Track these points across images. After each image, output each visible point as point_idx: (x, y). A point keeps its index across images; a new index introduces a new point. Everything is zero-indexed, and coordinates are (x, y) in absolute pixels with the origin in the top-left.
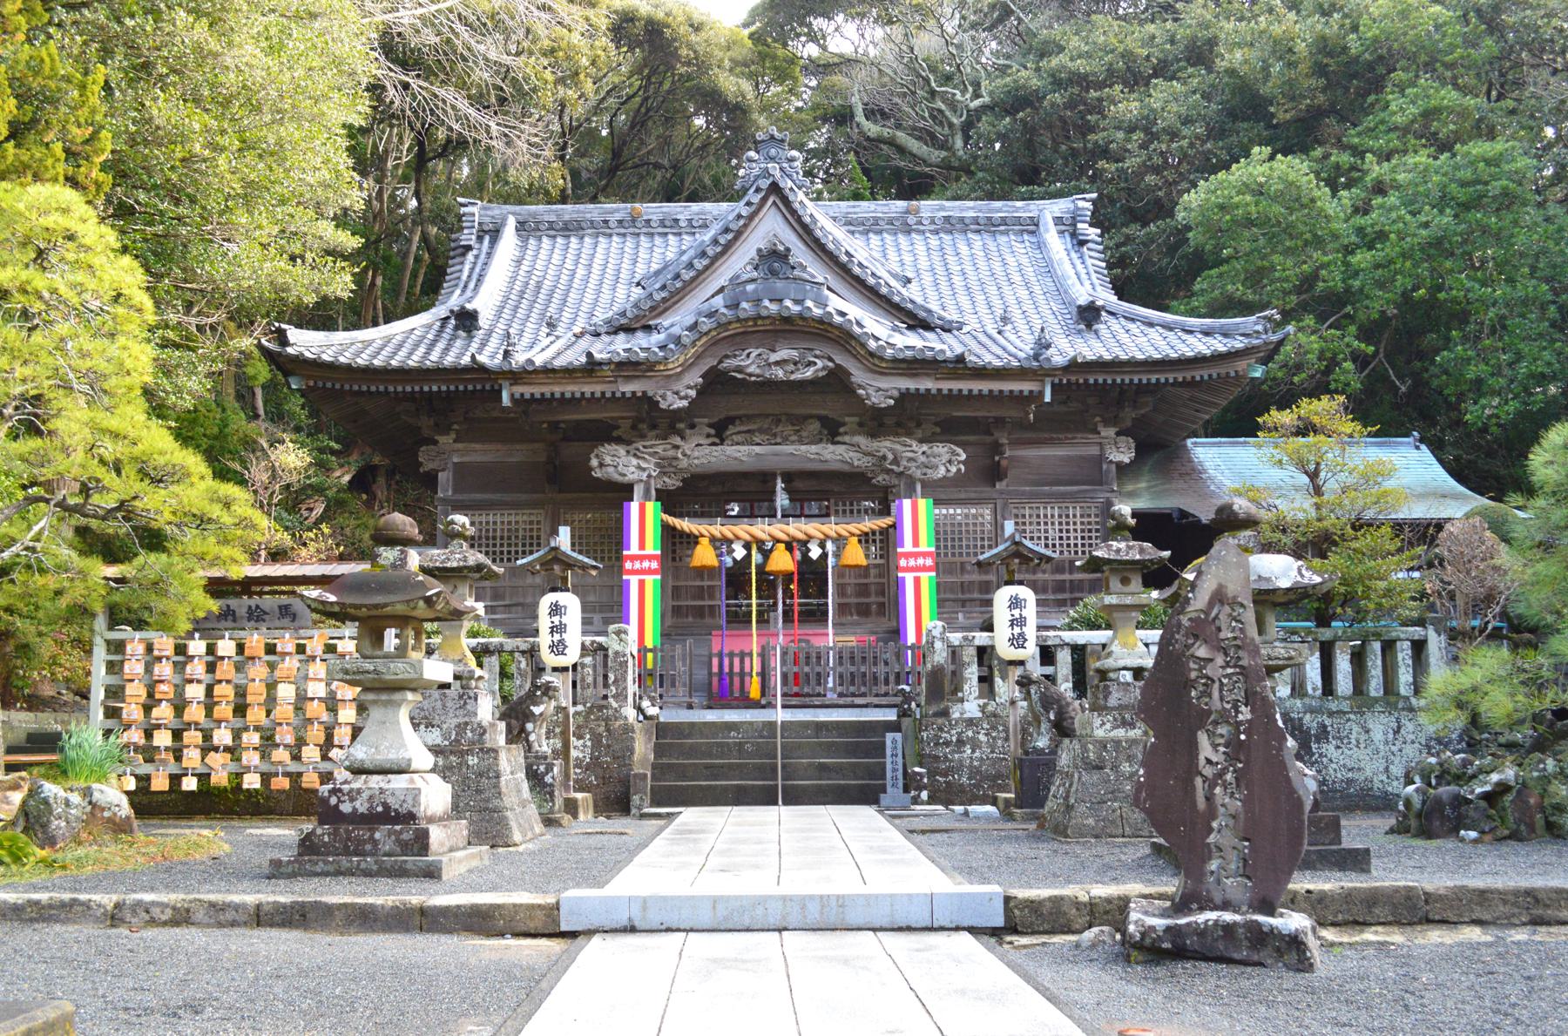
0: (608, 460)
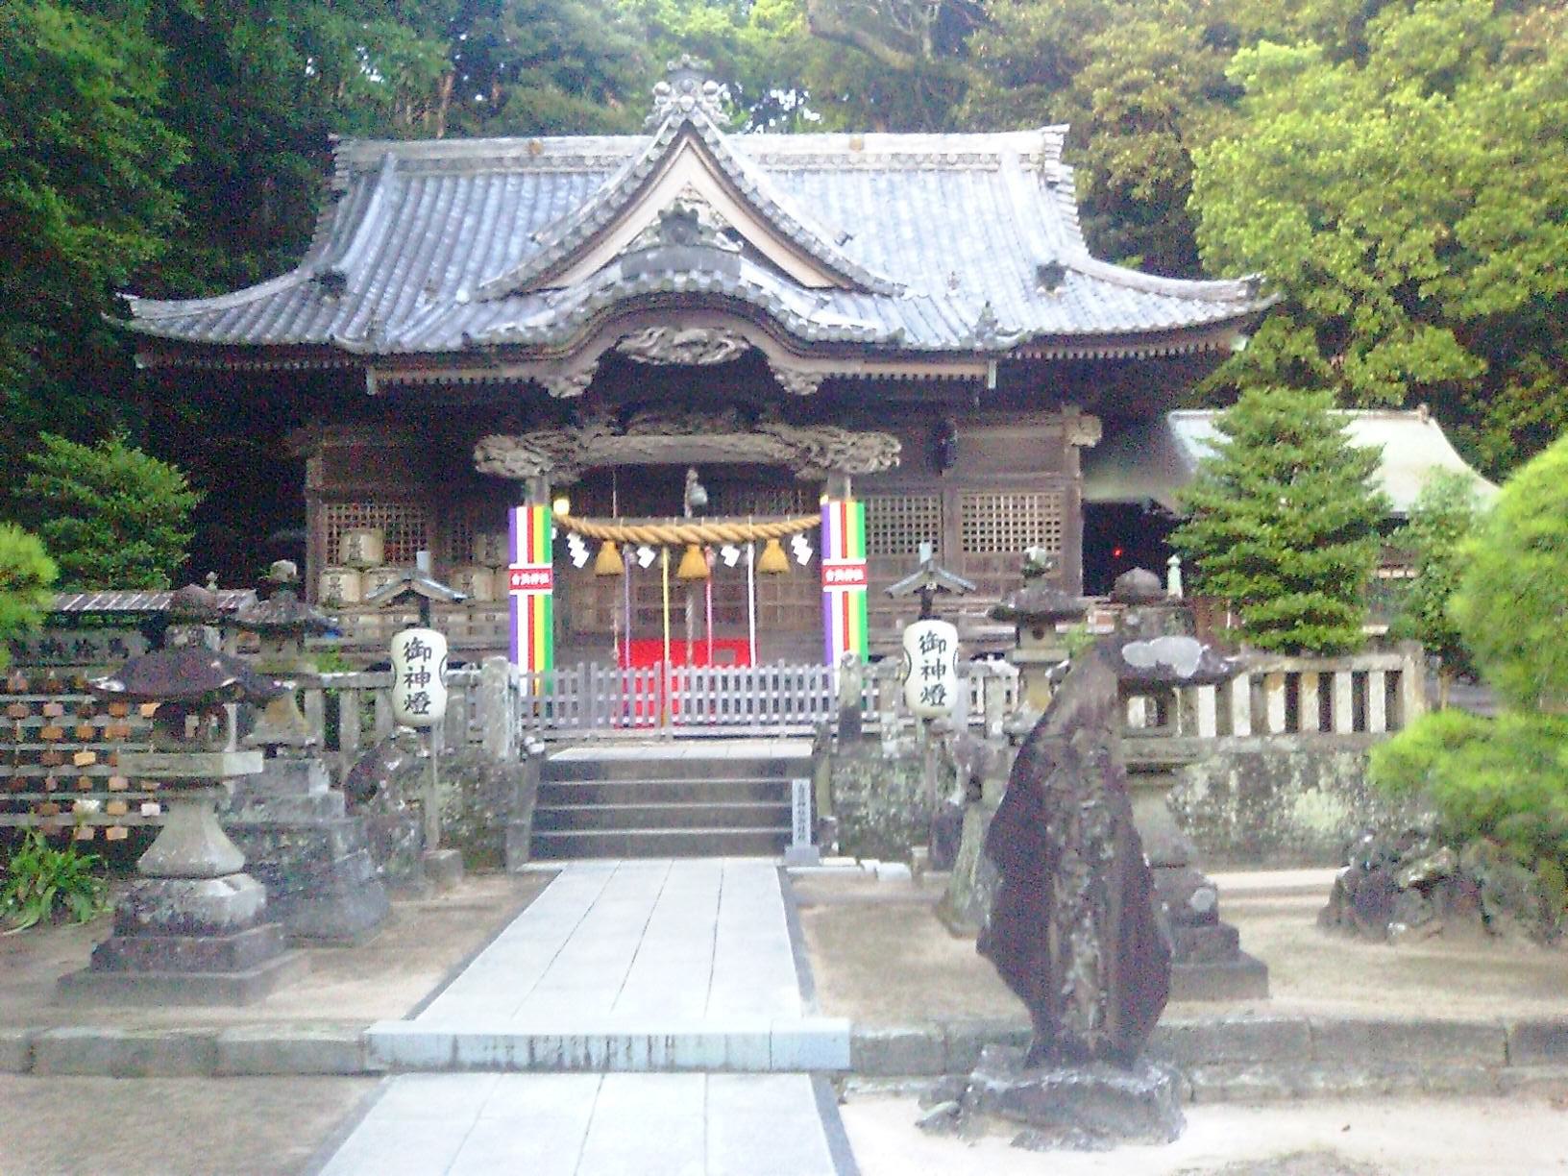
0: (494, 453)
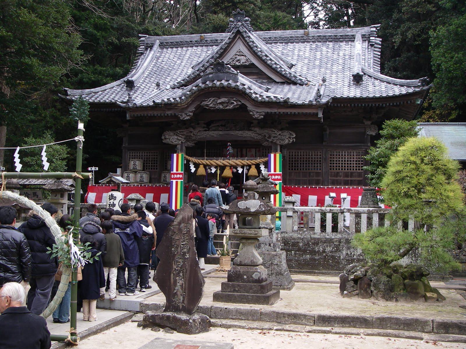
0: (167, 137)
